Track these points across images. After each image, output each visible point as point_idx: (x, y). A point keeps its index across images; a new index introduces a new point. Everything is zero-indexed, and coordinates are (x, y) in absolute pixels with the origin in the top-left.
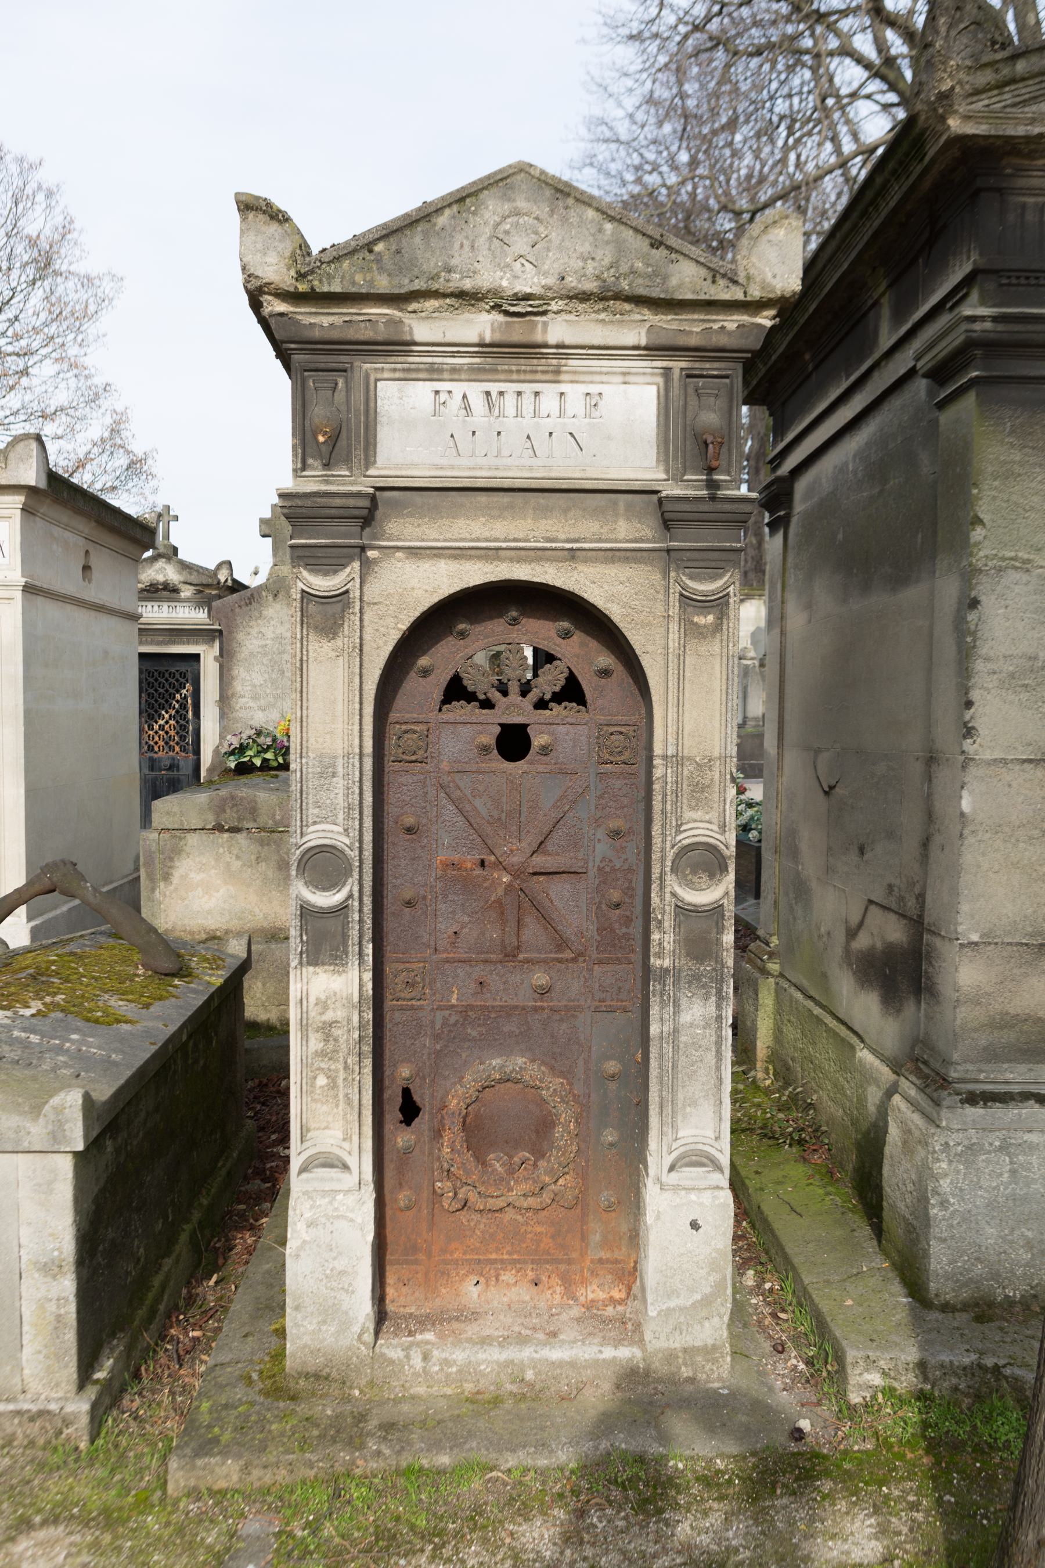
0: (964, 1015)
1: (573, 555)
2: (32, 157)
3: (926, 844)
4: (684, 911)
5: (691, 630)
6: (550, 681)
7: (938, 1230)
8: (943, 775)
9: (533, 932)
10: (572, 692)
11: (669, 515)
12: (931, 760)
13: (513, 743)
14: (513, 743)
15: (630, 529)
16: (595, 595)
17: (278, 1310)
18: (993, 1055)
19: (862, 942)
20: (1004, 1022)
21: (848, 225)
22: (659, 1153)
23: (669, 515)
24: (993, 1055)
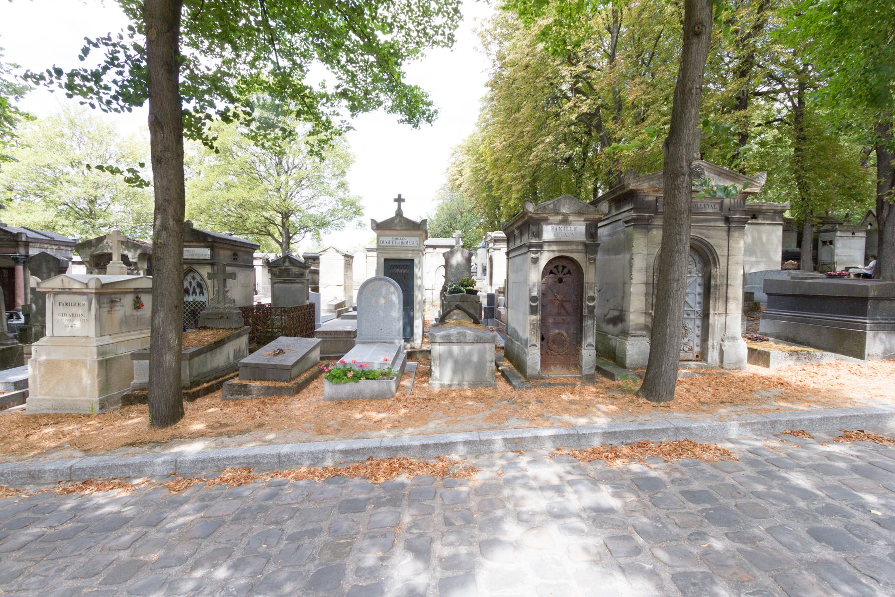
0: (631, 323)
1: (572, 252)
2: (402, 197)
3: (623, 297)
4: (589, 306)
5: (590, 263)
6: (566, 271)
7: (628, 356)
8: (626, 286)
9: (563, 311)
10: (569, 272)
11: (585, 245)
12: (624, 284)
13: (560, 280)
14: (560, 280)
15: (581, 248)
16: (575, 258)
17: (761, 296)
18: (635, 329)
19: (608, 316)
20: (637, 324)
21: (397, 263)
22: (584, 344)
23: (585, 245)
24: (635, 329)
